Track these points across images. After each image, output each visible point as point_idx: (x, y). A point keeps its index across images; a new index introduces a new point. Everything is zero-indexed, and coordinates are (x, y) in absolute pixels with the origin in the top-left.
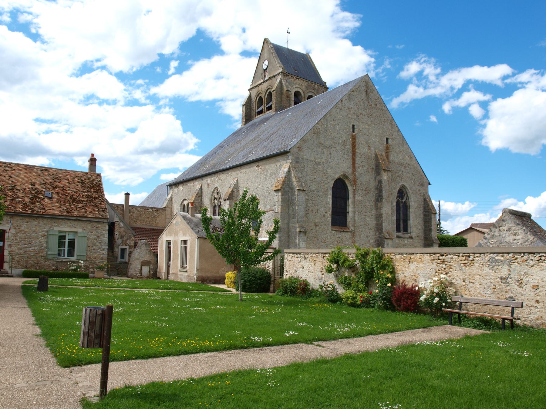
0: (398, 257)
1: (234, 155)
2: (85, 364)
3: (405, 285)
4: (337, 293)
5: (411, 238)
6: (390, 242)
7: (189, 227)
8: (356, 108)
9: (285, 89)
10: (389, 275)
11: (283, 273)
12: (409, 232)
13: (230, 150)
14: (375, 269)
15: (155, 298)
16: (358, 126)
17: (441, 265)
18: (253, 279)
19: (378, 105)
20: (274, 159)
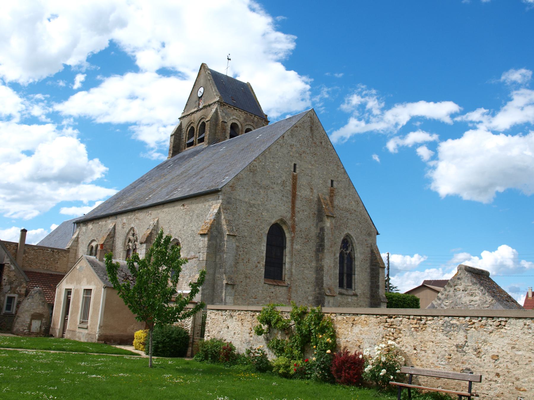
0: (339, 318)
3: (348, 352)
5: (355, 295)
6: (331, 300)
7: (95, 274)
8: (298, 146)
9: (221, 119)
10: (329, 340)
12: (353, 288)
15: (44, 361)
17: (389, 329)
18: (168, 340)
19: (323, 144)
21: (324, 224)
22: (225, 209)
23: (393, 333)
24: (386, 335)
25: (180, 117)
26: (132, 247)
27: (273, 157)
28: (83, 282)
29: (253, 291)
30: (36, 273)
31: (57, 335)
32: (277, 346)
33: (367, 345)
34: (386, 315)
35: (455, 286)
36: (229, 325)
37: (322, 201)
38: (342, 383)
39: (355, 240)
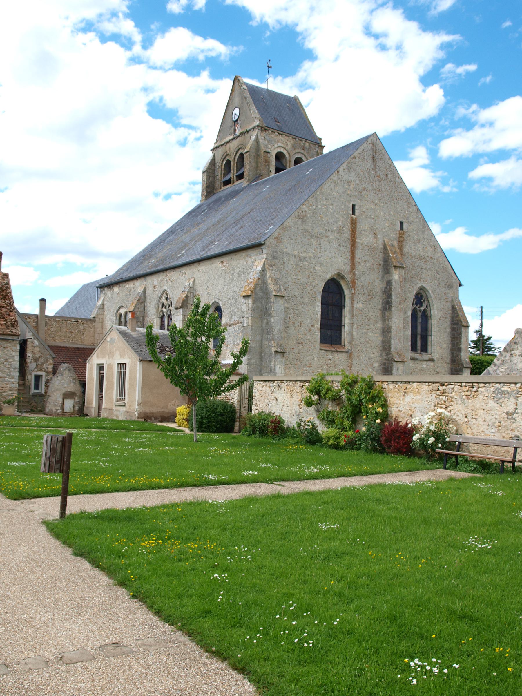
0: (391, 386)
1: (189, 247)
2: (33, 498)
3: (399, 422)
4: (317, 433)
5: (432, 360)
6: (401, 366)
7: (129, 346)
8: (358, 182)
9: (263, 149)
10: (380, 410)
11: (251, 408)
13: (186, 238)
14: (363, 401)
15: (89, 438)
16: (360, 206)
17: (441, 397)
18: (212, 415)
19: (389, 176)
20: (243, 254)
21: (392, 276)
22: (270, 265)
23: (445, 402)
24: (438, 404)
25: (212, 148)
26: (167, 313)
27: (326, 199)
28: (114, 356)
29: (308, 358)
30: (60, 347)
31: (93, 414)
33: (419, 414)
35: (511, 351)
36: (277, 397)
37: (388, 249)
38: (392, 452)
39: (432, 295)
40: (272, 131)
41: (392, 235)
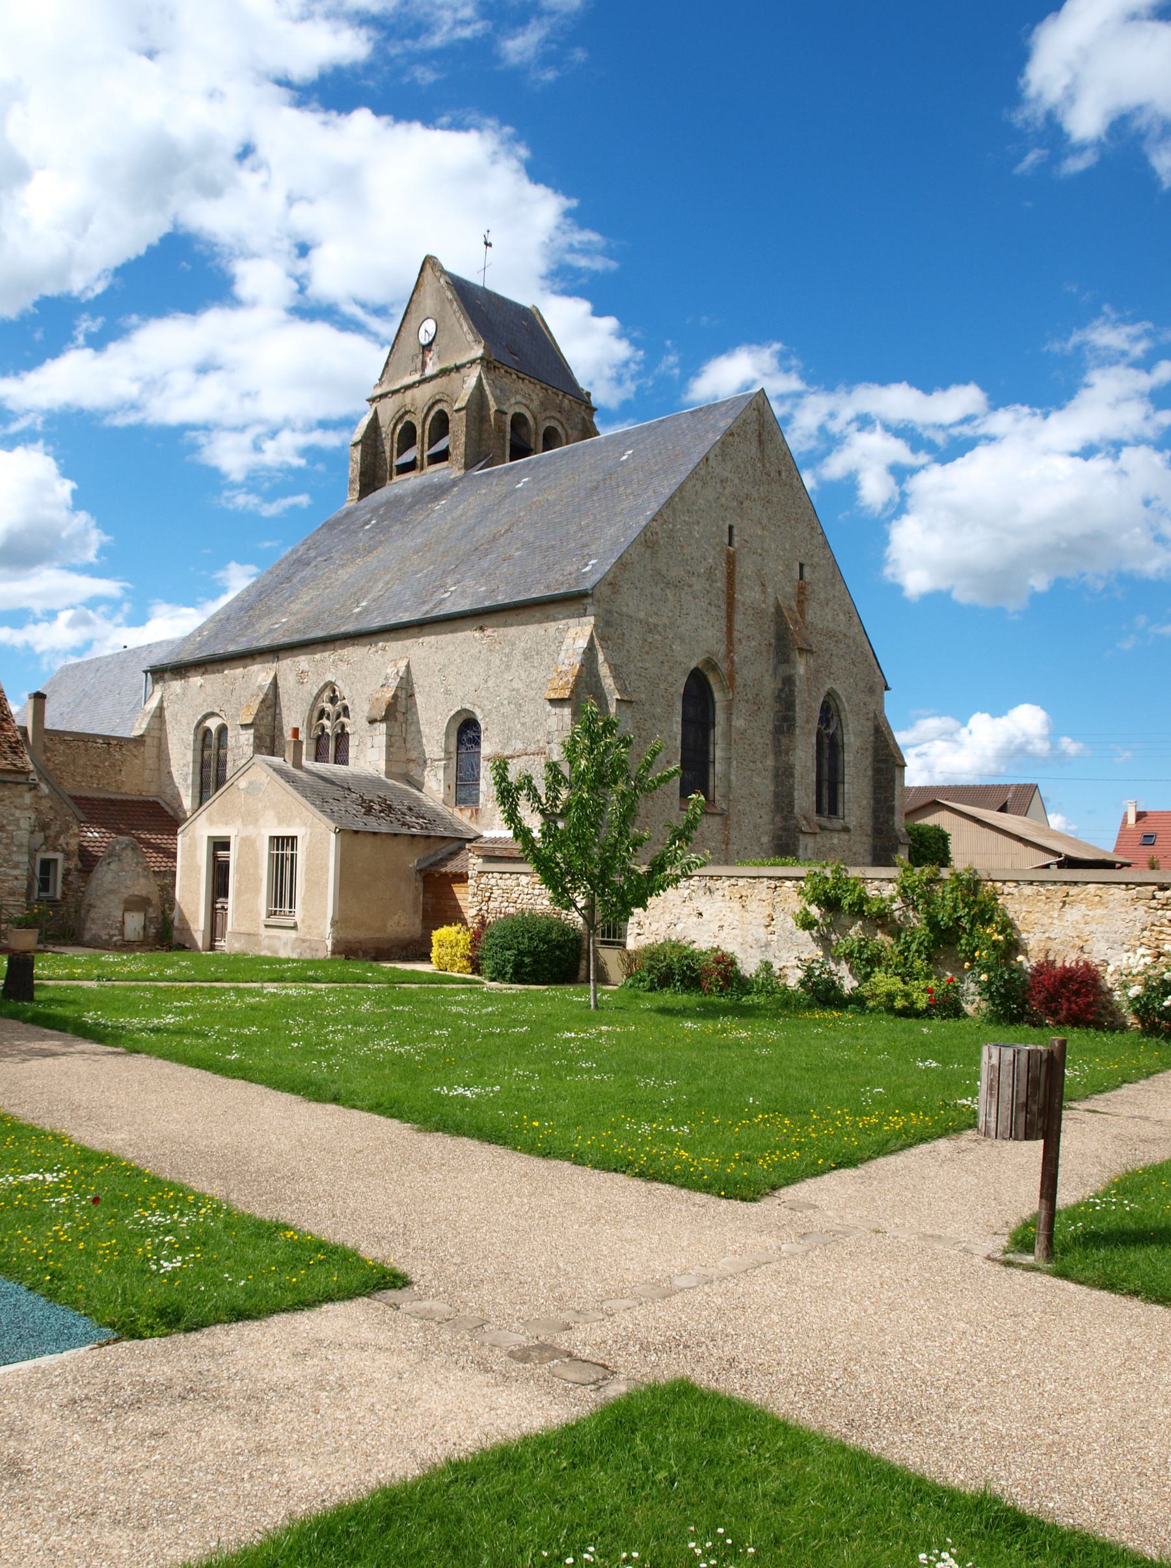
5: (846, 830)
8: (737, 481)
12: (840, 813)
17: (1160, 913)
19: (783, 474)
21: (794, 667)
24: (1153, 925)
32: (860, 952)
34: (1154, 884)
40: (506, 372)
41: (789, 589)
